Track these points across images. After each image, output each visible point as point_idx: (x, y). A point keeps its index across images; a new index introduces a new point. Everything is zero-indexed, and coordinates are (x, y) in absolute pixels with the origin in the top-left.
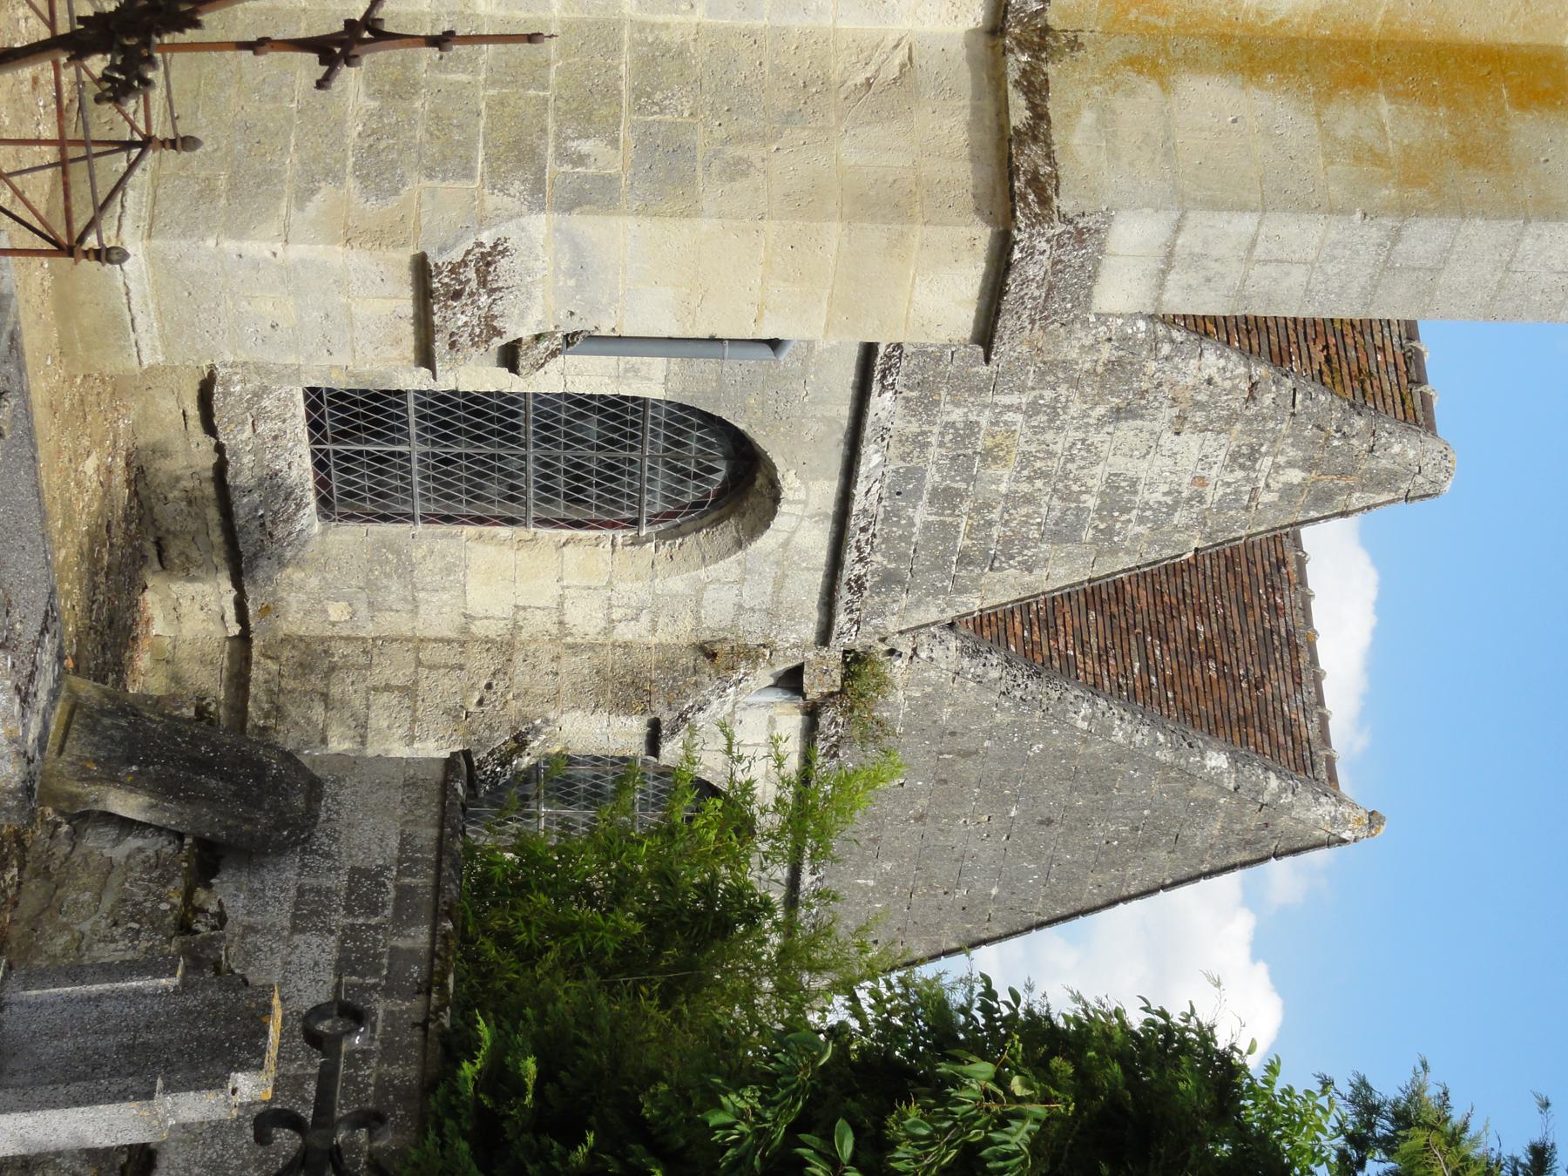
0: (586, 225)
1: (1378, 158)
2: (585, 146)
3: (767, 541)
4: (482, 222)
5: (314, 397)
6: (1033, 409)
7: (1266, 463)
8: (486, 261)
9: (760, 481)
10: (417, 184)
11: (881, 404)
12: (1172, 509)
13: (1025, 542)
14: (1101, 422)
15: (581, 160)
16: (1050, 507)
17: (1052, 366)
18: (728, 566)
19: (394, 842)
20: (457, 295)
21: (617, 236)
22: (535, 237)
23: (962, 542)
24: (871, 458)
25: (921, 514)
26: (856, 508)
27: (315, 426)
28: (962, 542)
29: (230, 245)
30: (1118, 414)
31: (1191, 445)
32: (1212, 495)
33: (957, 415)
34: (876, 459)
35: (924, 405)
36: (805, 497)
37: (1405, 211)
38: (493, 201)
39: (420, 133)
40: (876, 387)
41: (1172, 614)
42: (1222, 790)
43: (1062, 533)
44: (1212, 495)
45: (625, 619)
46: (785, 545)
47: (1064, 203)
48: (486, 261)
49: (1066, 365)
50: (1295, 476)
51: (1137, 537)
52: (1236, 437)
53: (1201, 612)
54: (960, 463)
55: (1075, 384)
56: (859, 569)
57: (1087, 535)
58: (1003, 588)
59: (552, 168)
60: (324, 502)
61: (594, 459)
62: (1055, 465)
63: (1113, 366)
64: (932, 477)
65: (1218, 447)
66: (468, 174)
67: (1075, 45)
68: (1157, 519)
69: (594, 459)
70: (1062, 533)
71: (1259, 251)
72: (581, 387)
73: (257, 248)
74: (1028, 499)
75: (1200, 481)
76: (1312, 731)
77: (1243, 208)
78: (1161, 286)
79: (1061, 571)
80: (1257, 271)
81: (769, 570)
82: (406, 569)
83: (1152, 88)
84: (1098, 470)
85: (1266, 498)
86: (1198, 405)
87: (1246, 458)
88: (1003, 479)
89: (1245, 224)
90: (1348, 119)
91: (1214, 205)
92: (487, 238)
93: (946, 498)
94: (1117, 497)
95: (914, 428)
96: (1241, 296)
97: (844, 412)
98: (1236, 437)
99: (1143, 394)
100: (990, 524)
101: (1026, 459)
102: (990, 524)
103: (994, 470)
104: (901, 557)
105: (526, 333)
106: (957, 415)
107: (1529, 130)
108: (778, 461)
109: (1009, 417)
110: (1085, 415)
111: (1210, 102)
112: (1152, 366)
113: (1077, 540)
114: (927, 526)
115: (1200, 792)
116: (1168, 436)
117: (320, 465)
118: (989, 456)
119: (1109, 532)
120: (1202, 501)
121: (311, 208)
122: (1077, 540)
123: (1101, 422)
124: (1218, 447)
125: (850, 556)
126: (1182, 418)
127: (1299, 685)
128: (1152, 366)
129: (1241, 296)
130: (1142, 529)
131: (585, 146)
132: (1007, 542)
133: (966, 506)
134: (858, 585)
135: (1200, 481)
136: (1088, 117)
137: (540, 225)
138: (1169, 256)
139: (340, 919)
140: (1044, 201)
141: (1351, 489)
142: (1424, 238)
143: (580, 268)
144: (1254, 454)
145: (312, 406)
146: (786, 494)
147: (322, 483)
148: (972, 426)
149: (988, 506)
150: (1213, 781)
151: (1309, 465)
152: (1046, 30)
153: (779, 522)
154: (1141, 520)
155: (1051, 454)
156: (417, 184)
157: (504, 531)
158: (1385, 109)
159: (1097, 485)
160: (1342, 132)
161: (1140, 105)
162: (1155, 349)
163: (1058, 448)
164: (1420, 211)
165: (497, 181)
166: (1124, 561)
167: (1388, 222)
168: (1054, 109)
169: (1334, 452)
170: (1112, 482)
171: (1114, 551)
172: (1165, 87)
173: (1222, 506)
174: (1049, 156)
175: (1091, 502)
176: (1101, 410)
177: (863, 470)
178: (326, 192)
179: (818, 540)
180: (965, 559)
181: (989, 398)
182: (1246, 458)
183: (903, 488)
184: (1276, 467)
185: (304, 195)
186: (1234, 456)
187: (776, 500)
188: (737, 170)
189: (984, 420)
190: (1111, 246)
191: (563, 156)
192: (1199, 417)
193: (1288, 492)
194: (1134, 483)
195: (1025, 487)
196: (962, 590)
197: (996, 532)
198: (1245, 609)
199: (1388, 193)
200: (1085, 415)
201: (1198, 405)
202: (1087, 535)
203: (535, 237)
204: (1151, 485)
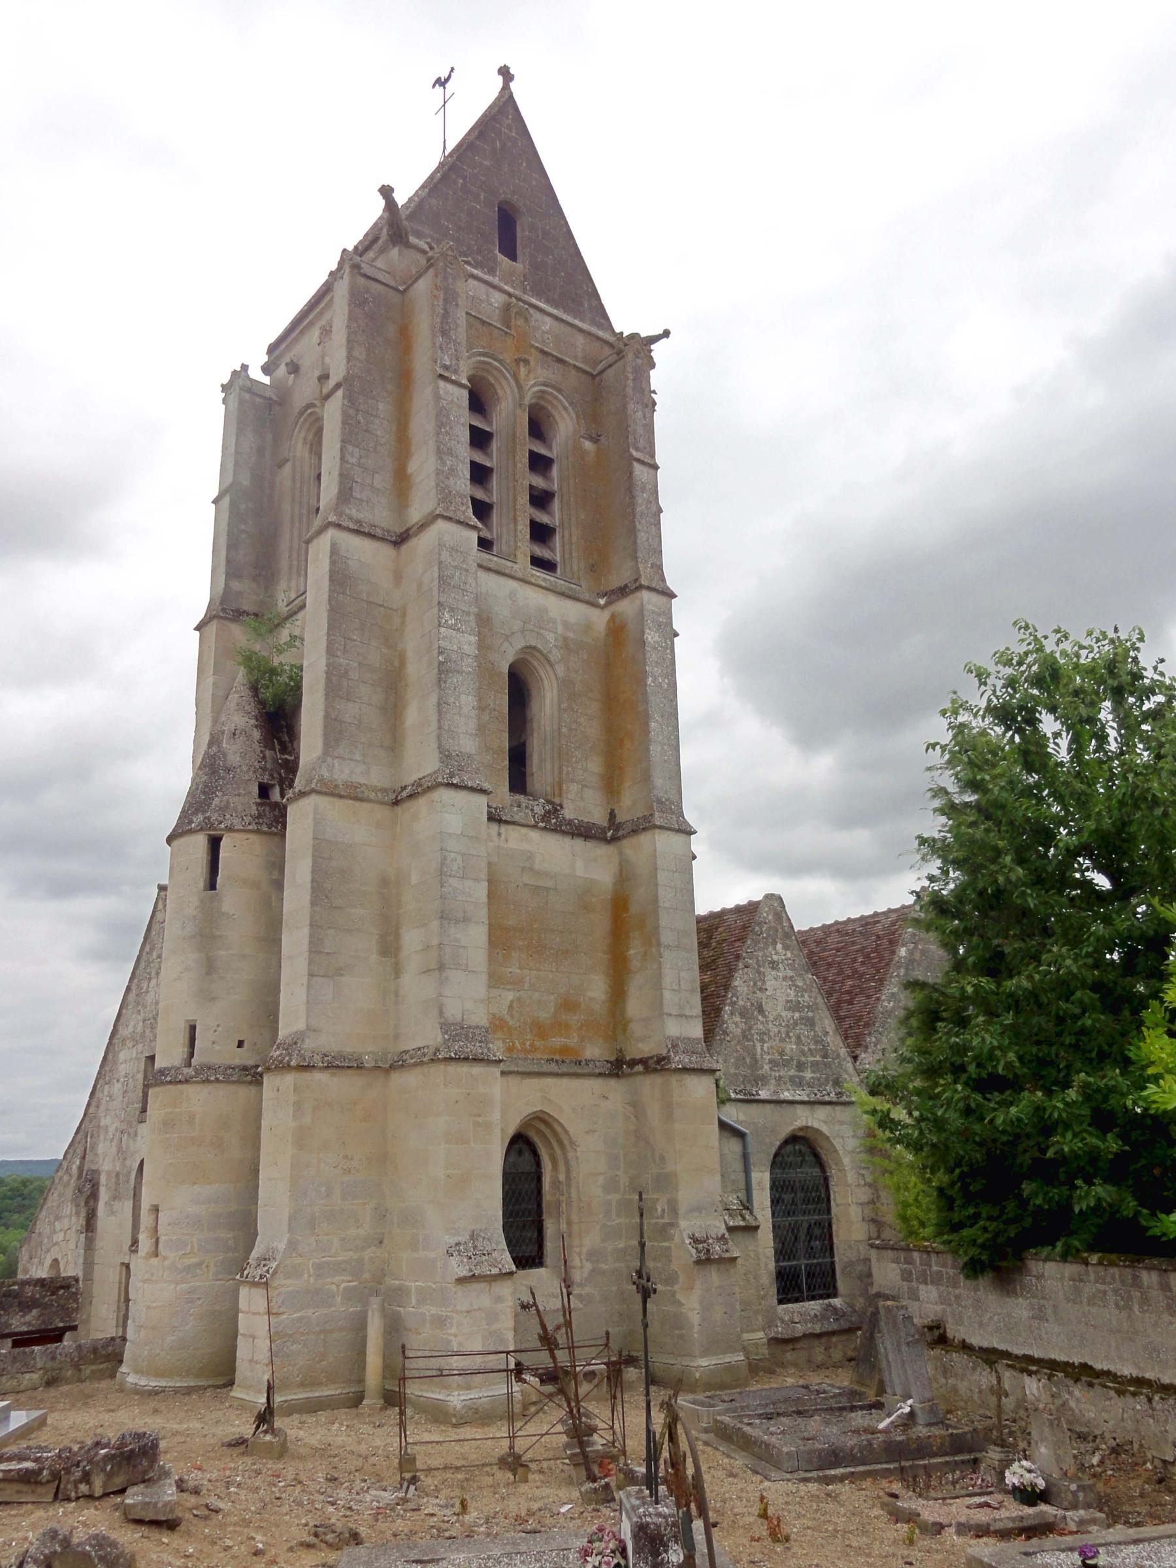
0: (682, 1209)
1: (645, 953)
2: (659, 1210)
3: (825, 1129)
4: (683, 1242)
5: (780, 1302)
6: (762, 1041)
7: (775, 958)
8: (696, 1241)
9: (801, 1134)
10: (674, 1266)
11: (764, 1094)
12: (797, 986)
13: (816, 1036)
14: (765, 1016)
15: (663, 1210)
16: (802, 1030)
17: (745, 1037)
18: (837, 1143)
19: (894, 1265)
20: (708, 1251)
21: (686, 1196)
22: (688, 1226)
23: (818, 1058)
24: (786, 1095)
25: (808, 1075)
26: (806, 1099)
27: (797, 1300)
28: (818, 1058)
29: (696, 1329)
30: (761, 1010)
31: (770, 984)
32: (790, 973)
33: (766, 1067)
34: (786, 1094)
35: (762, 1080)
36: (803, 1118)
37: (659, 945)
38: (677, 1239)
39: (659, 1265)
40: (757, 1097)
41: (855, 971)
42: (915, 948)
43: (811, 1023)
44: (790, 973)
45: (864, 1179)
46: (825, 1122)
47: (664, 1053)
48: (696, 1241)
49: (743, 1032)
50: (779, 946)
51: (810, 997)
52: (766, 970)
53: (854, 960)
54: (786, 1064)
55: (750, 1028)
56: (833, 1095)
57: (810, 1014)
58: (834, 1042)
59: (666, 1220)
60: (829, 1296)
61: (800, 1195)
62: (783, 1030)
63: (742, 1015)
64: (792, 1072)
65: (770, 975)
66: (669, 1248)
67: (621, 1051)
68: (800, 991)
69: (800, 1195)
70: (811, 1023)
71: (676, 988)
72: (768, 1202)
73: (695, 1318)
74: (798, 1037)
75: (785, 978)
76: (894, 916)
77: (661, 995)
78: (691, 1017)
79: (827, 1023)
80: (683, 987)
81: (837, 1127)
82: (851, 1264)
83: (631, 1025)
84: (783, 1014)
85: (789, 954)
86: (755, 984)
87: (774, 965)
88: (791, 1047)
89: (667, 994)
90: (635, 964)
91: (661, 1004)
92: (688, 1241)
93: (800, 1067)
94: (795, 1007)
95: (773, 1081)
96: (692, 991)
97: (768, 1106)
98: (766, 970)
99: (752, 1004)
100: (810, 1050)
101: (782, 1040)
102: (810, 1050)
103: (788, 1051)
104: (827, 1080)
105: (724, 1227)
106: (766, 1067)
107: (634, 909)
108: (791, 1128)
109: (765, 1049)
110: (762, 1023)
111: (635, 1006)
112: (741, 1003)
113: (813, 1018)
114: (813, 1072)
115: (917, 956)
116: (768, 993)
117: (813, 1298)
118: (782, 1053)
119: (808, 1007)
120: (792, 977)
121: (683, 1301)
122: (813, 1018)
123: (765, 1016)
124: (770, 975)
125: (827, 1098)
126: (760, 989)
127: (878, 922)
128: (741, 1003)
129: (692, 991)
130: (806, 996)
131: (659, 1210)
132: (816, 1042)
133: (803, 1059)
134: (839, 1094)
135: (785, 978)
136: (640, 1045)
137: (683, 1224)
138: (680, 1016)
139: (914, 1284)
140: (664, 1058)
141: (783, 928)
142: (667, 937)
143: (698, 1209)
144: (773, 962)
145: (789, 1301)
146: (804, 1124)
147: (821, 1297)
148: (771, 1061)
149: (802, 1052)
150: (911, 952)
151: (775, 943)
152: (617, 1060)
153: (816, 1125)
154: (802, 996)
155: (779, 1032)
156: (674, 1266)
157: (834, 1227)
158: (632, 952)
159: (790, 1014)
160: (638, 964)
161: (636, 1029)
162: (735, 1003)
163: (776, 1030)
164: (658, 940)
165: (670, 1238)
166: (819, 1000)
167: (662, 950)
168: (638, 1057)
169: (769, 935)
170: (790, 1009)
171: (816, 1004)
172: (630, 1021)
173: (793, 969)
174: (652, 1058)
175: (797, 1015)
176: (760, 1017)
177: (791, 1098)
178: (679, 1297)
179: (822, 1112)
180: (825, 1056)
181: (758, 1056)
182: (774, 965)
183: (798, 1083)
184: (776, 953)
185: (680, 1304)
186: (773, 968)
187: (807, 1127)
188: (662, 1159)
189: (767, 1057)
190: (678, 1034)
191: (662, 1217)
192: (759, 984)
193: (786, 948)
194: (788, 1002)
195: (793, 1039)
196: (838, 1056)
197: (813, 1047)
198: (853, 943)
199: (654, 950)
200: (762, 1023)
201: (755, 984)
202: (810, 1014)
203: (688, 1226)
204: (788, 995)
